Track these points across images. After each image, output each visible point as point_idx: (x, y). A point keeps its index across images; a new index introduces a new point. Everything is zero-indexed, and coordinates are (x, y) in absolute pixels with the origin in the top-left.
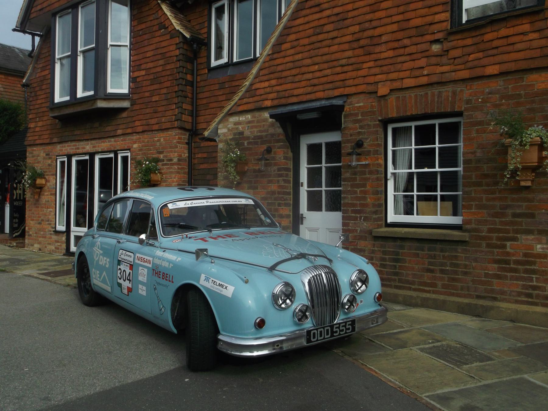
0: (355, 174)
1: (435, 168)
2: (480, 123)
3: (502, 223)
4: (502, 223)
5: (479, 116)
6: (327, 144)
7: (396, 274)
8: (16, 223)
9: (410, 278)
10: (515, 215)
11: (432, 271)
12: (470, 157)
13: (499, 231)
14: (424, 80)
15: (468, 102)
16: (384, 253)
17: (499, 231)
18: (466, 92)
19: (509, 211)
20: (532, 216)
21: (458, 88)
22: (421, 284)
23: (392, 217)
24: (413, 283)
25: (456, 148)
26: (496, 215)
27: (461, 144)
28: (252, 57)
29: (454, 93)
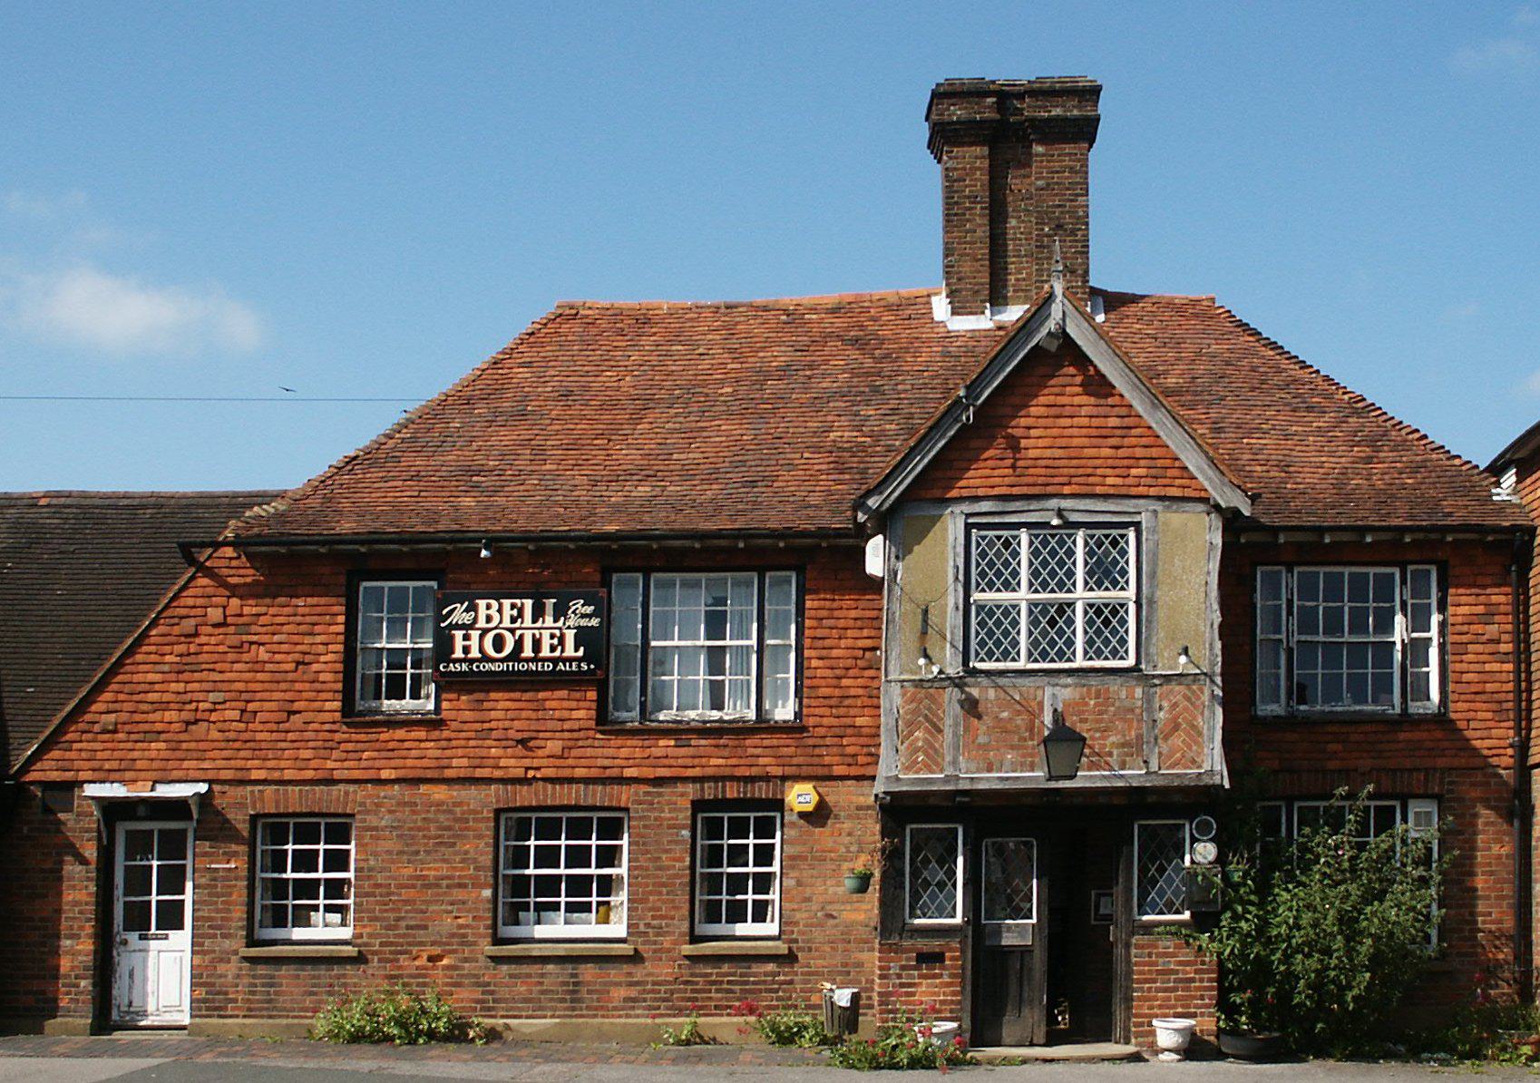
0: (215, 879)
1: (558, 866)
2: (376, 829)
3: (396, 936)
4: (396, 936)
5: (372, 820)
6: (160, 831)
7: (269, 1001)
8: (935, 1012)
9: (289, 1005)
10: (408, 927)
11: (315, 994)
12: (362, 864)
13: (392, 944)
14: (309, 774)
15: (362, 804)
16: (254, 977)
17: (392, 944)
18: (359, 793)
19: (403, 924)
20: (426, 927)
21: (351, 788)
22: (302, 1009)
23: (958, 920)
24: (293, 1010)
25: (348, 851)
26: (388, 928)
27: (625, 842)
28: (1410, 568)
29: (347, 793)
